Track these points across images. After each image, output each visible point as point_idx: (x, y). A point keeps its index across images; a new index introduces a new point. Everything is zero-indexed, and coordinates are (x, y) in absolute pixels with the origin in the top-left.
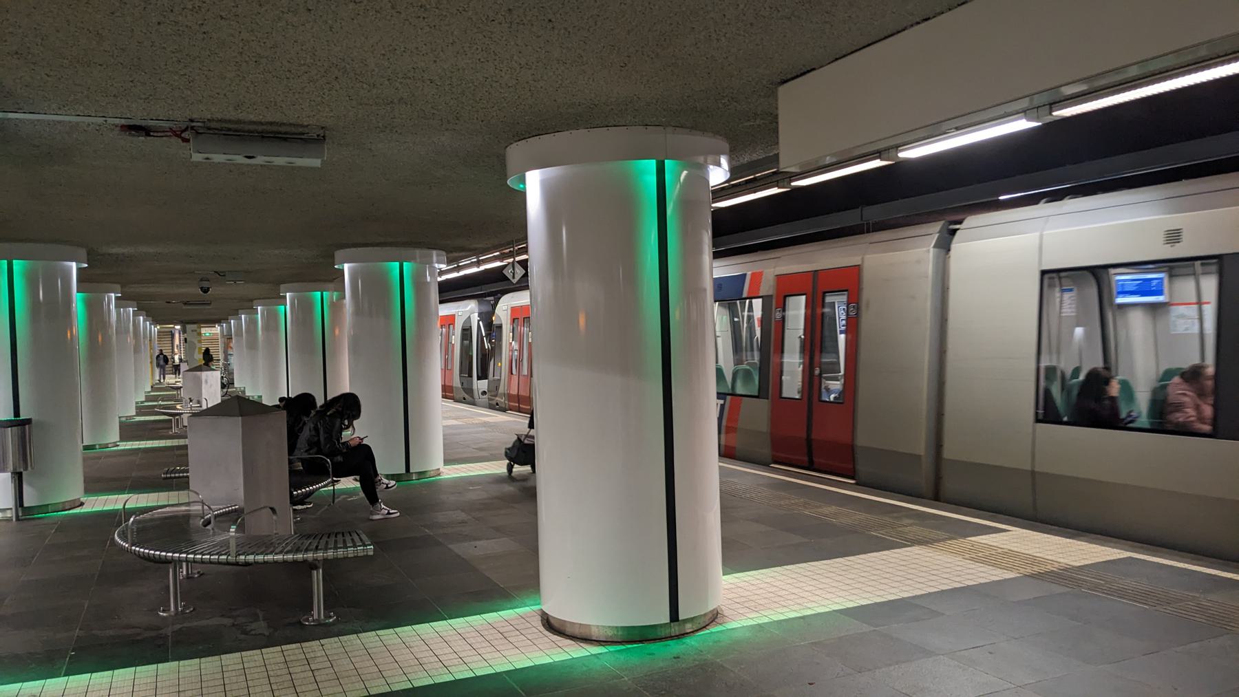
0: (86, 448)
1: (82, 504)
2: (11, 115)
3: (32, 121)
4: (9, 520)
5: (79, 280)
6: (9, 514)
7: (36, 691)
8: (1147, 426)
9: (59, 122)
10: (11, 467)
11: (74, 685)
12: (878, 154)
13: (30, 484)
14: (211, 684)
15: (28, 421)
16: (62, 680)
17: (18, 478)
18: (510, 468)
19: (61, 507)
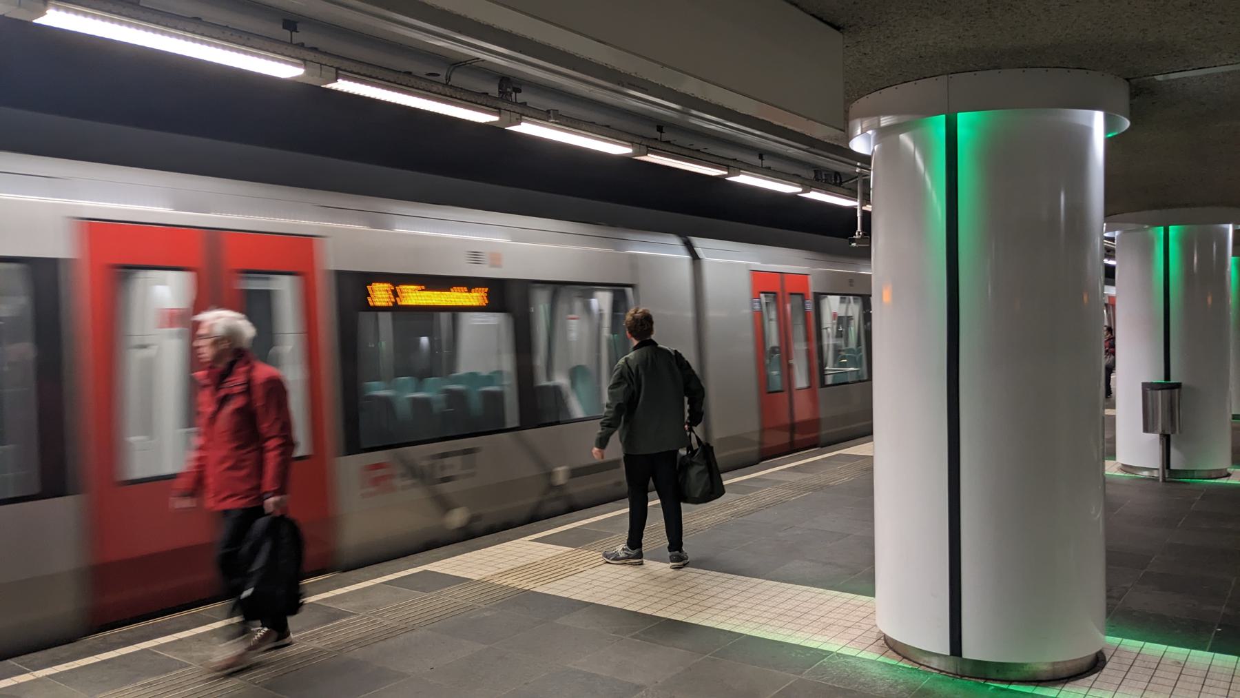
0: (1235, 417)
1: (1228, 475)
2: (1173, 76)
3: (1201, 78)
4: (1156, 480)
5: (1235, 244)
6: (1156, 474)
7: (1182, 659)
8: (516, 424)
9: (1228, 73)
10: (1160, 429)
11: (1220, 663)
12: (287, 33)
13: (1178, 448)
14: (1167, 682)
15: (1178, 386)
16: (1207, 655)
17: (1166, 441)
18: (792, 437)
19: (1206, 475)
